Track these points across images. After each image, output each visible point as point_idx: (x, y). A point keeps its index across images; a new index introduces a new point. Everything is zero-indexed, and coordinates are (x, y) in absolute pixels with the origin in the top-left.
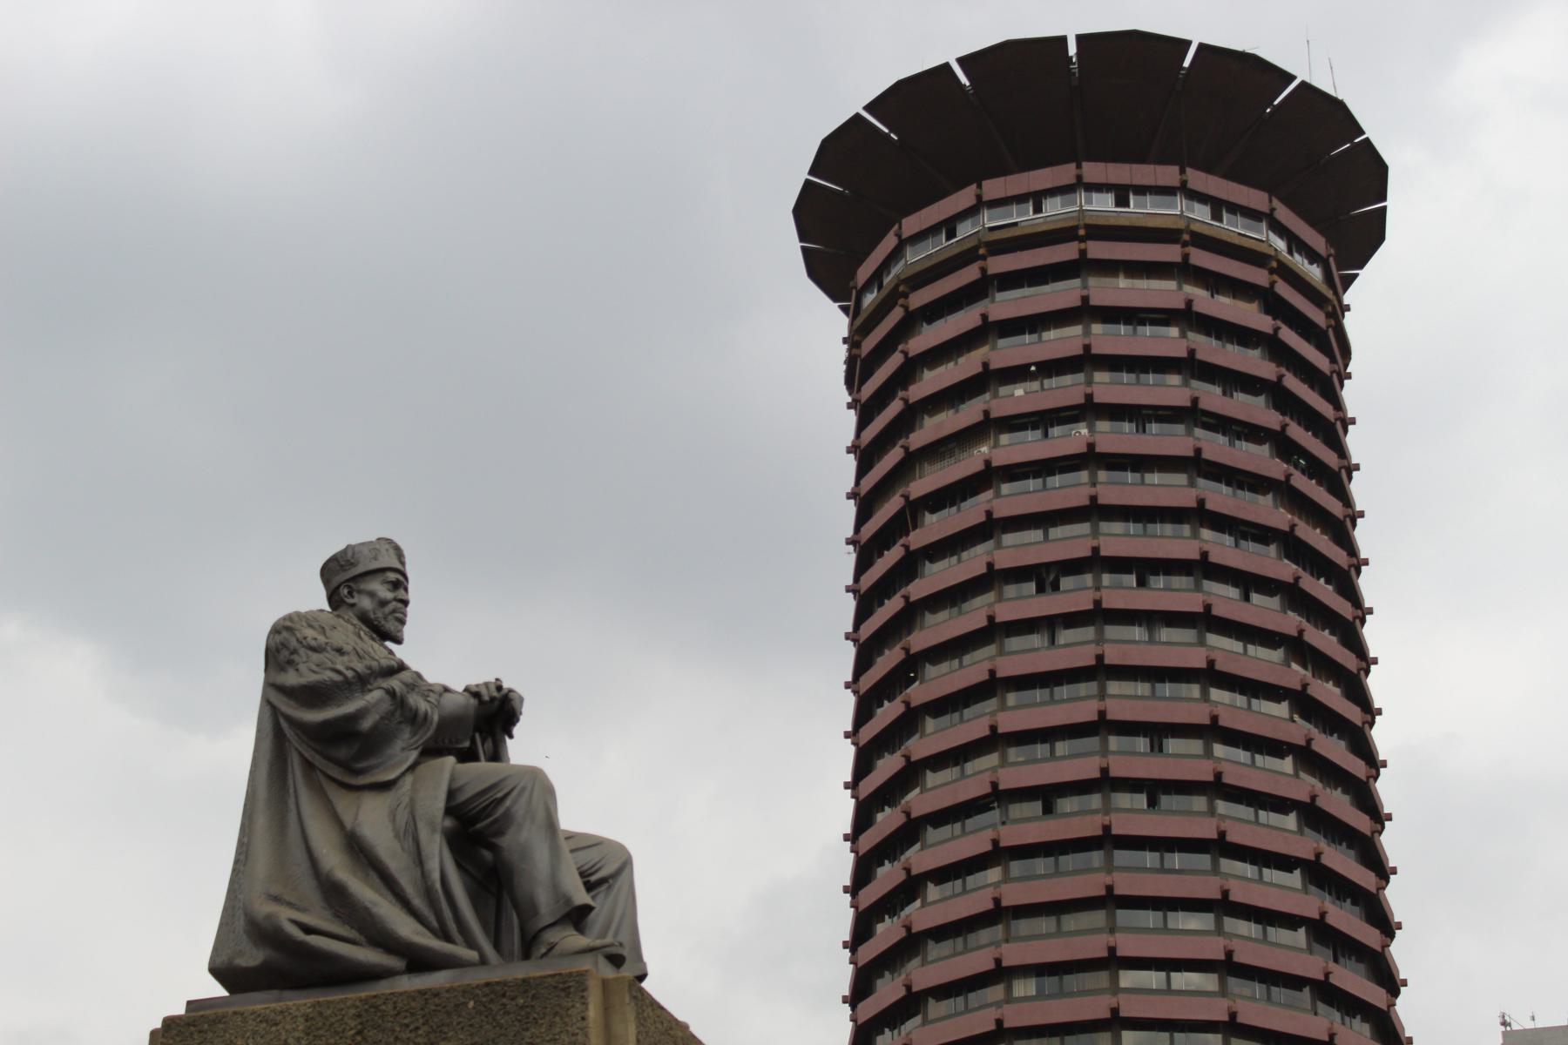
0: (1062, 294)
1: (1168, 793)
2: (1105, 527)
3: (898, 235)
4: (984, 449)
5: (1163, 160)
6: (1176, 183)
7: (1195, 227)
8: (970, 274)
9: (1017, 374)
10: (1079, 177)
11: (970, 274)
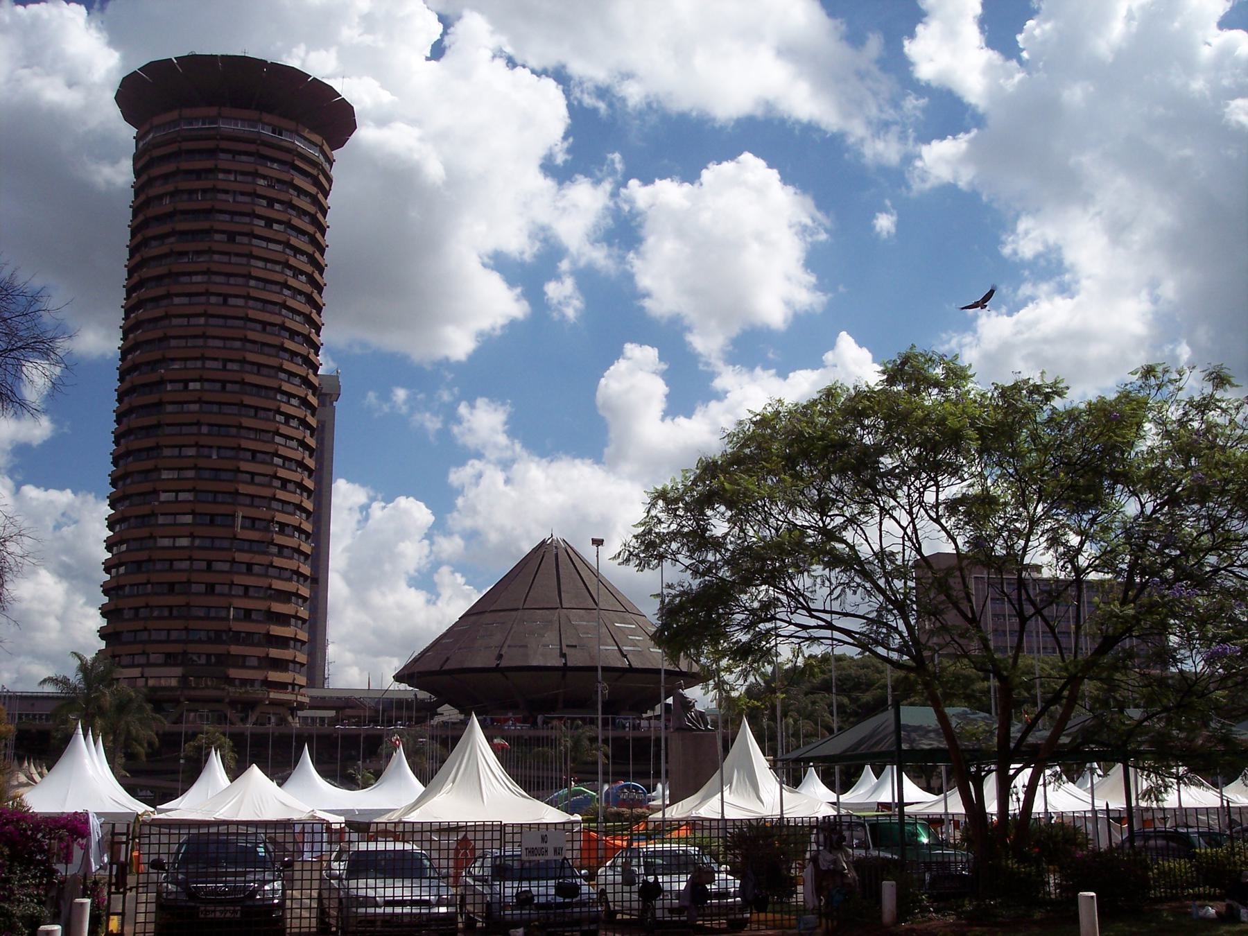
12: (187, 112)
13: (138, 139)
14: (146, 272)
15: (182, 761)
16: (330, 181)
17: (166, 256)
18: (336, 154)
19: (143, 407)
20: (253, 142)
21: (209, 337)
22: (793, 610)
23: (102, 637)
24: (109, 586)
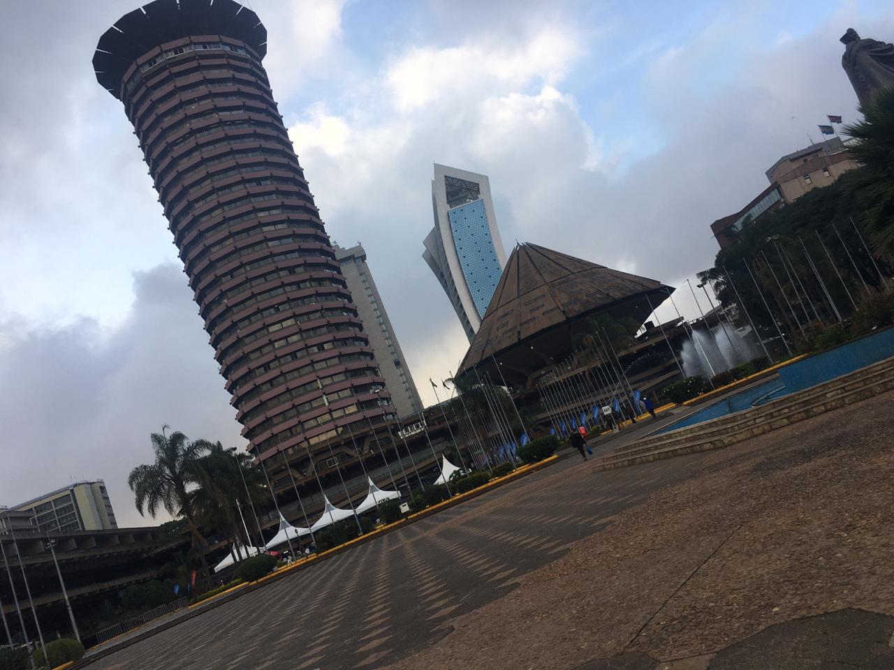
0: (196, 77)
1: (228, 236)
2: (203, 150)
3: (137, 64)
4: (225, 301)
5: (182, 37)
6: (189, 42)
7: (199, 54)
8: (166, 74)
9: (191, 102)
10: (191, 41)
11: (166, 74)
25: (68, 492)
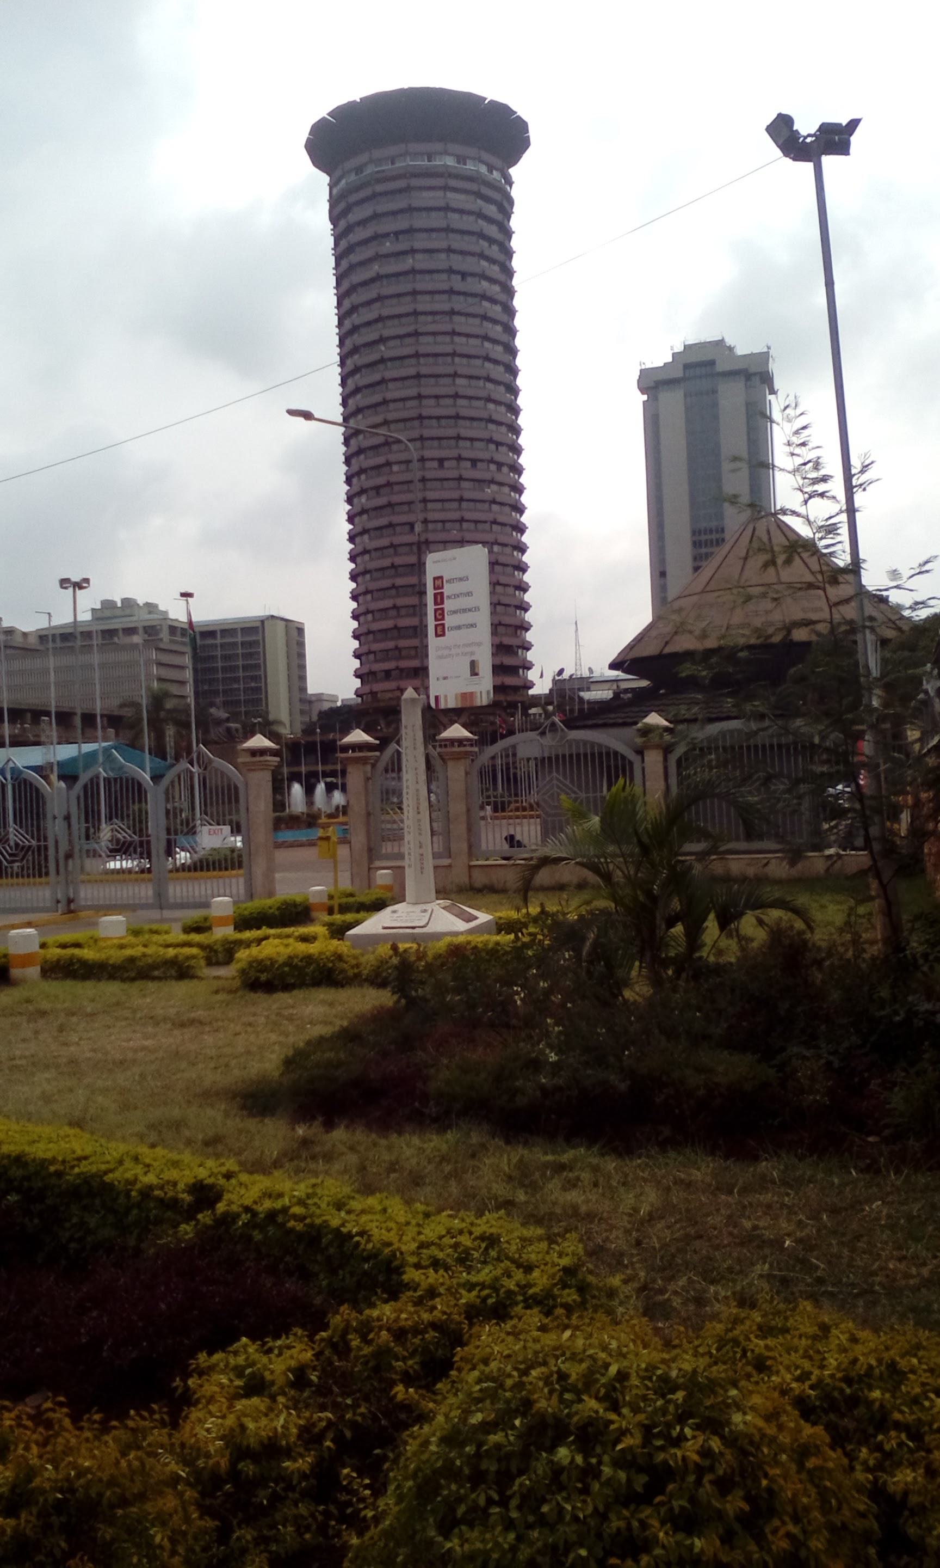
12: (377, 154)
13: (331, 186)
14: (354, 238)
15: (439, 1499)
16: (511, 202)
17: (373, 280)
18: (513, 171)
19: (367, 386)
20: (440, 175)
21: (422, 334)
22: (701, 1350)
23: (357, 676)
24: (354, 553)
25: (259, 624)
